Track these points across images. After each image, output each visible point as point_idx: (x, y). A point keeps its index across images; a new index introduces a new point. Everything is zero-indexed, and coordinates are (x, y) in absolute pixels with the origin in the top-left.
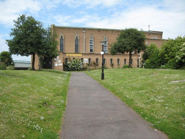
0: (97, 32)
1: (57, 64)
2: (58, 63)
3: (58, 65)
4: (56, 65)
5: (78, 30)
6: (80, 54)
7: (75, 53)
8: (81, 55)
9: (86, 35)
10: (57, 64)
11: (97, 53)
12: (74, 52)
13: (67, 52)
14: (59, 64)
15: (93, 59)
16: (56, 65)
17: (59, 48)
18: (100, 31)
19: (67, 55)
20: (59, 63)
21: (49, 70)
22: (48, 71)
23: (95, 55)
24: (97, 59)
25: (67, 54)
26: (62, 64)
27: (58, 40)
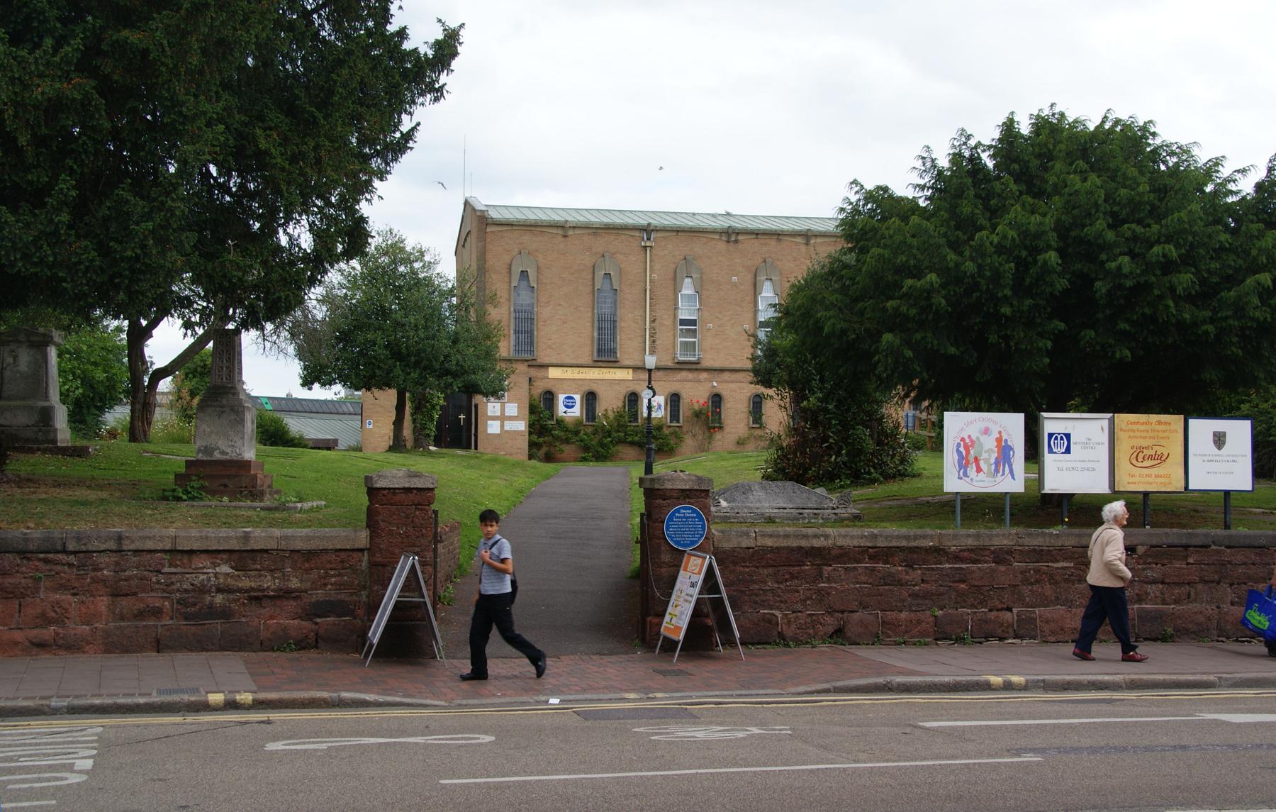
0: (722, 246)
1: (498, 423)
2: (502, 418)
3: (502, 426)
4: (493, 428)
5: (612, 238)
6: (625, 371)
7: (597, 364)
8: (626, 375)
9: (657, 267)
10: (498, 423)
11: (717, 365)
12: (586, 355)
13: (554, 361)
14: (509, 426)
15: (695, 393)
16: (490, 431)
17: (505, 348)
18: (740, 237)
19: (554, 373)
20: (511, 418)
21: (460, 452)
22: (458, 456)
23: (704, 375)
24: (717, 399)
25: (199, 562)
26: (521, 426)
27: (499, 314)
